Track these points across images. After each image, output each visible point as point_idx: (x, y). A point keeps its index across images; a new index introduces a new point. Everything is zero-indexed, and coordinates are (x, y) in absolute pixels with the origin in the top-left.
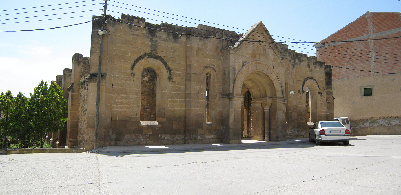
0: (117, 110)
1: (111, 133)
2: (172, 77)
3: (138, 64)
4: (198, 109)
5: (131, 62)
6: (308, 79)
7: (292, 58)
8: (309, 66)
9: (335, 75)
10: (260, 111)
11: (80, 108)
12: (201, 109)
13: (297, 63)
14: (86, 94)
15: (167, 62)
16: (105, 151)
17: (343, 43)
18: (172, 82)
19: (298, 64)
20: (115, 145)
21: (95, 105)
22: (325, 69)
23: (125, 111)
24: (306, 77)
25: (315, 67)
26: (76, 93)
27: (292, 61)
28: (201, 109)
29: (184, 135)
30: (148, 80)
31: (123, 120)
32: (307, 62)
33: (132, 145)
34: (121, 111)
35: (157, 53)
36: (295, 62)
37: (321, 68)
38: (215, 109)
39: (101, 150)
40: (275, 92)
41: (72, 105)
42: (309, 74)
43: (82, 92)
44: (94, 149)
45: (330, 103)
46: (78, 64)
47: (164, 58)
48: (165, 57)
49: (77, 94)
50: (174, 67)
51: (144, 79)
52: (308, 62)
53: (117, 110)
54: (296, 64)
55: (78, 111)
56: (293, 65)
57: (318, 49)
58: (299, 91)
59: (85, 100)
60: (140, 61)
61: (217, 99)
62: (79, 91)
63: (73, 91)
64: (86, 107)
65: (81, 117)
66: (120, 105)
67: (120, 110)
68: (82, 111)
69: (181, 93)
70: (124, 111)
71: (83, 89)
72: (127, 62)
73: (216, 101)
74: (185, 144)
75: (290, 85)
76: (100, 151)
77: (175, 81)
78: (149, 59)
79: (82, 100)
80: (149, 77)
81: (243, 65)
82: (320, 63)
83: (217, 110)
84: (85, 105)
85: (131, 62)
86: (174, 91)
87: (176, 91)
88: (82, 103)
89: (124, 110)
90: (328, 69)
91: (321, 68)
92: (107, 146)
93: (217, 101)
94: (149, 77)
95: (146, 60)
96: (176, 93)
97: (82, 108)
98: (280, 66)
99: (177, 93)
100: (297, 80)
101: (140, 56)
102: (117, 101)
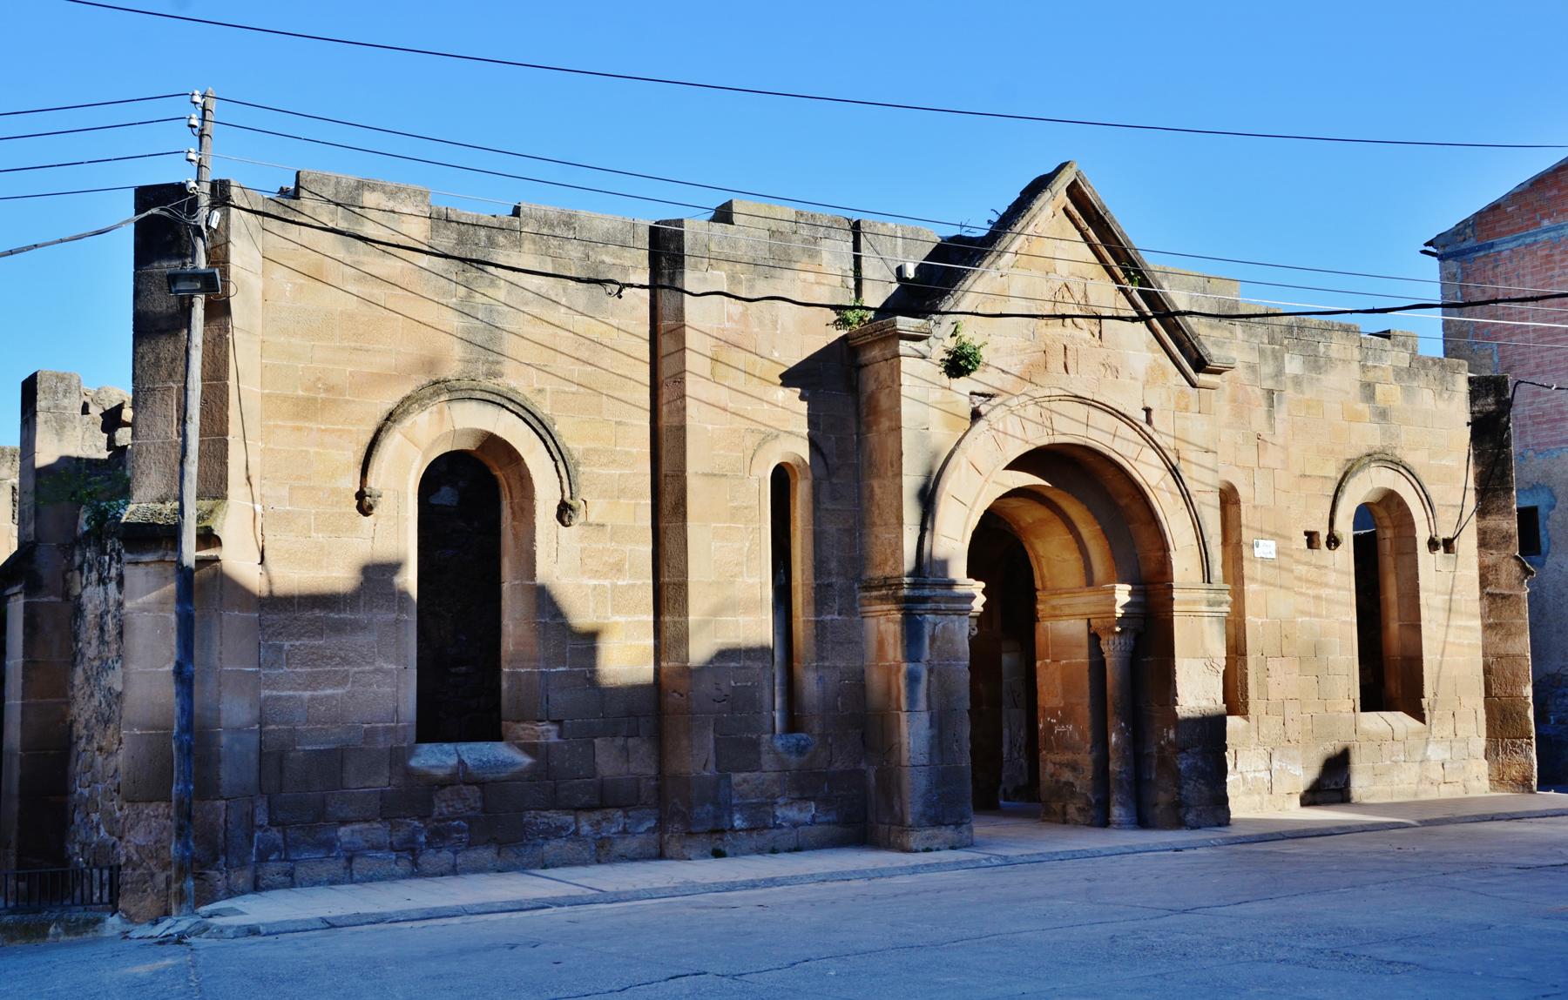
0: (291, 693)
1: (261, 818)
2: (585, 492)
3: (392, 444)
4: (733, 664)
5: (354, 429)
6: (1362, 467)
7: (1261, 352)
8: (1368, 390)
9: (1556, 420)
10: (1082, 658)
11: (79, 676)
12: (749, 668)
13: (1296, 376)
14: (111, 602)
15: (552, 419)
16: (229, 927)
17: (579, 882)
18: (587, 524)
19: (1305, 384)
20: (283, 886)
21: (172, 679)
22: (1474, 396)
23: (332, 697)
24: (1354, 454)
25: (1408, 393)
26: (53, 598)
27: (1267, 369)
28: (749, 663)
29: (657, 811)
30: (455, 503)
31: (327, 747)
32: (1355, 366)
33: (380, 880)
34: (313, 699)
35: (501, 375)
36: (1279, 373)
37: (1446, 396)
38: (827, 664)
39: (210, 920)
40: (1160, 553)
41: (30, 664)
42: (1369, 436)
43: (89, 589)
44: (167, 914)
45: (1504, 597)
46: (58, 434)
47: (539, 398)
48: (540, 391)
49: (60, 600)
50: (593, 445)
51: (434, 500)
52: (1363, 367)
53: (291, 693)
54: (1290, 384)
55: (65, 695)
56: (1271, 392)
57: (1453, 266)
58: (1311, 537)
59: (106, 638)
60: (407, 422)
61: (836, 607)
62: (65, 580)
63: (33, 588)
64: (114, 680)
65: (84, 732)
66: (303, 664)
67: (307, 694)
68: (92, 695)
69: (633, 586)
70: (327, 697)
71: (94, 576)
72: (334, 431)
73: (829, 617)
74: (661, 856)
75: (1255, 507)
76: (206, 929)
77: (600, 521)
78: (457, 406)
79: (89, 633)
80: (461, 483)
81: (976, 415)
82: (1437, 368)
83: (834, 667)
84: (105, 667)
85: (354, 429)
86: (595, 574)
87: (605, 576)
88: (91, 652)
89: (329, 692)
90: (1490, 400)
91: (1446, 396)
92: (243, 893)
93: (836, 617)
94: (461, 483)
95: (440, 412)
96: (607, 583)
97: (87, 679)
98: (1186, 409)
99: (614, 586)
100: (1298, 473)
101: (408, 398)
102: (287, 645)
